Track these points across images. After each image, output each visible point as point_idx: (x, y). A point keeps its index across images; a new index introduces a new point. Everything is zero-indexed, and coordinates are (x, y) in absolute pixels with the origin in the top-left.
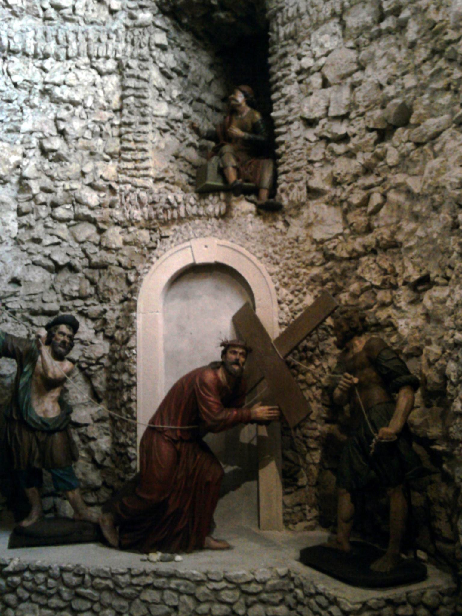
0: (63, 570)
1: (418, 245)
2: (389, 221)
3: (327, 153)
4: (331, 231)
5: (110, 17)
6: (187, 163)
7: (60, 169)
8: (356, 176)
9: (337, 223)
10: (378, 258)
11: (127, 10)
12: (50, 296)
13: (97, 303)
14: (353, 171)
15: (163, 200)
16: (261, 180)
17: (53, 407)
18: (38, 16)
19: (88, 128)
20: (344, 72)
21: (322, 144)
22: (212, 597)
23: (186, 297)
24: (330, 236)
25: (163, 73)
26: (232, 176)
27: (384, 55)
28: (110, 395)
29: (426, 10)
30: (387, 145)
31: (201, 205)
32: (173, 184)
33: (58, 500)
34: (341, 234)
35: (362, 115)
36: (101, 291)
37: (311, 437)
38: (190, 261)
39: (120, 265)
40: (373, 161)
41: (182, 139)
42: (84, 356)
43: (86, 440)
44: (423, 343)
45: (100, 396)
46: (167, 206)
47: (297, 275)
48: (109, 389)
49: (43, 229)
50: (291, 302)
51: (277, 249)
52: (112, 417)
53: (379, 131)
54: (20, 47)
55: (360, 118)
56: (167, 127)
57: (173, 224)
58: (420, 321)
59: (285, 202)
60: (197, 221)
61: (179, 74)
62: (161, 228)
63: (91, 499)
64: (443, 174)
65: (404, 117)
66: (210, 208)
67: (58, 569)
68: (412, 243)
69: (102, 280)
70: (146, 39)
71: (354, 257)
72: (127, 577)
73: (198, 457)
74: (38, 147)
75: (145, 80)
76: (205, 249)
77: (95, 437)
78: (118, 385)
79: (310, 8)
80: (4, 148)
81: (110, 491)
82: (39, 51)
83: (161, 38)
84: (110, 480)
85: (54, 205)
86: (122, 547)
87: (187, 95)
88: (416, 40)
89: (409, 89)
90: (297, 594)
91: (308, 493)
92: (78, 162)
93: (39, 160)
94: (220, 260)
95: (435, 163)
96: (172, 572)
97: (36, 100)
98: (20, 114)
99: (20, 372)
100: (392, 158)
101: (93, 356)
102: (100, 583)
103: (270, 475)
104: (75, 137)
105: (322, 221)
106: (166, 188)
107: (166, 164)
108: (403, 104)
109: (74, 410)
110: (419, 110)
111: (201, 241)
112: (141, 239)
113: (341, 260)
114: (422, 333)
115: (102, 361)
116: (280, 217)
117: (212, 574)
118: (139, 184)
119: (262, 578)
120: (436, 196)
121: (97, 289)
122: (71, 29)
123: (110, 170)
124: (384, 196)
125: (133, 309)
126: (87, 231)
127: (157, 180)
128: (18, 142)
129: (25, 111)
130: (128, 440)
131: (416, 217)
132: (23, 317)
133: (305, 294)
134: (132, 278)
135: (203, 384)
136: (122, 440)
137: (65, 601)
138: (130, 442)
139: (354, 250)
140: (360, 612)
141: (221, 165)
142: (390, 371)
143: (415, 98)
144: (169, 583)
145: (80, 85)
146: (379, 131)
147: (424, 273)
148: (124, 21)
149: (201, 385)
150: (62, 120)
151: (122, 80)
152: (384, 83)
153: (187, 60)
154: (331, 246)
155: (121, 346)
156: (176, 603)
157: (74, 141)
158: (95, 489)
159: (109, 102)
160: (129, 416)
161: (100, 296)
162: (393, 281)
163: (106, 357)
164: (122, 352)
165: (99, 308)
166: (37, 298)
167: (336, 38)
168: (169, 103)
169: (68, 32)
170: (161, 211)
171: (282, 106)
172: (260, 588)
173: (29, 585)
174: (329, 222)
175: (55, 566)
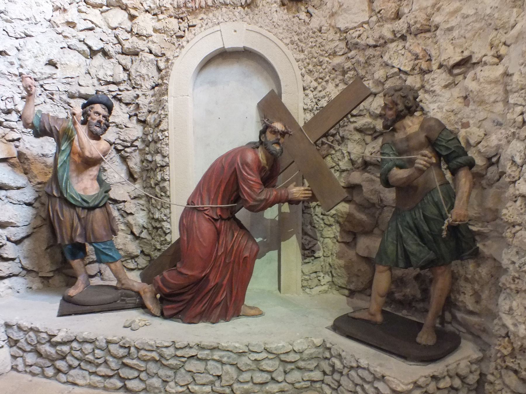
0: (108, 342)
4: (356, 20)
9: (363, 11)
10: (407, 45)
12: (85, 80)
13: (130, 88)
17: (92, 185)
22: (254, 366)
23: (213, 83)
24: (356, 25)
28: (144, 176)
34: (367, 23)
36: (134, 77)
38: (218, 46)
39: (151, 52)
43: (125, 215)
44: (459, 126)
45: (136, 176)
47: (321, 63)
48: (144, 170)
50: (315, 88)
51: (302, 37)
52: (147, 196)
57: (200, 13)
58: (457, 105)
60: (224, 9)
62: (188, 17)
63: (131, 265)
67: (105, 341)
69: (134, 66)
71: (381, 44)
73: (236, 235)
77: (133, 212)
78: (152, 166)
81: (148, 258)
86: (163, 316)
91: (322, 263)
94: (249, 45)
96: (215, 345)
101: (128, 139)
103: (291, 247)
109: (112, 189)
112: (170, 26)
114: (459, 116)
115: (135, 144)
119: (300, 348)
121: (129, 75)
125: (165, 92)
130: (162, 215)
132: (61, 99)
133: (327, 81)
134: (162, 65)
135: (245, 163)
136: (157, 216)
138: (165, 218)
142: (448, 150)
144: (212, 355)
147: (466, 54)
149: (242, 165)
154: (357, 34)
155: (154, 129)
158: (133, 257)
160: (163, 194)
161: (133, 82)
162: (424, 66)
163: (139, 140)
164: (155, 134)
165: (133, 93)
166: (74, 82)
172: (298, 357)
173: (78, 354)
175: (100, 338)
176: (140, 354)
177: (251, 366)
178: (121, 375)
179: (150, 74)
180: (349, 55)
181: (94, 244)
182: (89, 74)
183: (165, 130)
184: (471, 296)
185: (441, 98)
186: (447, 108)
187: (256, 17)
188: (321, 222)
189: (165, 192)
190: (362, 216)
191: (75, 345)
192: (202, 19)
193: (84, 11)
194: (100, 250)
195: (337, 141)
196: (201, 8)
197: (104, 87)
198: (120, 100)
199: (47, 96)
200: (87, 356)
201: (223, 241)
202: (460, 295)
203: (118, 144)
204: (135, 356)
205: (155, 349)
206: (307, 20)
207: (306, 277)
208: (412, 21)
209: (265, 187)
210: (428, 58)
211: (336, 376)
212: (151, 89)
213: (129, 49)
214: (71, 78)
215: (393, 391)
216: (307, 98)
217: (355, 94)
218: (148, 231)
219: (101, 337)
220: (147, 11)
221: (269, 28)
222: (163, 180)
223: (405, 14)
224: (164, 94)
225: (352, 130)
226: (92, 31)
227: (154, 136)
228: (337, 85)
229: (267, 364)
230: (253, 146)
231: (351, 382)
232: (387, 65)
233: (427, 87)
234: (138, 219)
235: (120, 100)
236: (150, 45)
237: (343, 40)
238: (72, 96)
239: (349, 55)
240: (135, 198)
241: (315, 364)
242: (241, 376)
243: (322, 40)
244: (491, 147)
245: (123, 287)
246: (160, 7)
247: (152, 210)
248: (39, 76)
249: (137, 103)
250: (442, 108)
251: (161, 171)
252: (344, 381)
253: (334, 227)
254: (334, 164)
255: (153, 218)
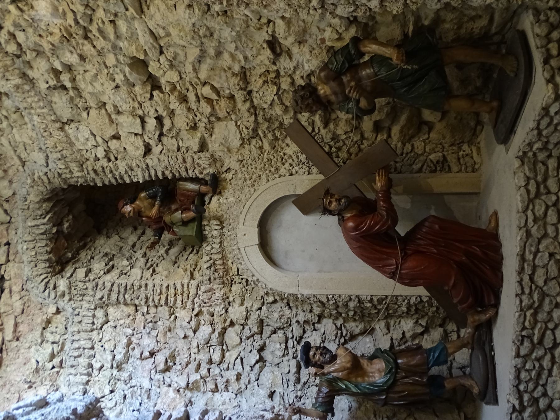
0: (518, 355)
1: (243, 52)
2: (224, 78)
3: (171, 135)
5: (62, 314)
6: (181, 254)
7: (182, 356)
8: (189, 109)
10: (255, 89)
11: (57, 299)
13: (291, 328)
14: (185, 111)
15: (208, 272)
16: (193, 191)
18: (58, 372)
19: (150, 333)
20: (107, 120)
21: (164, 139)
22: (541, 223)
24: (238, 131)
25: (109, 271)
26: (191, 214)
27: (92, 85)
28: (368, 319)
29: (53, 45)
30: (163, 81)
31: (212, 241)
32: (196, 266)
33: (455, 364)
34: (236, 123)
35: (140, 104)
37: (403, 149)
38: (257, 249)
39: (260, 309)
40: (176, 94)
41: (162, 258)
42: (334, 340)
43: (404, 340)
46: (212, 269)
47: (269, 160)
48: (362, 319)
49: (229, 371)
50: (291, 165)
51: (248, 177)
53: (153, 89)
54: (81, 387)
55: (143, 106)
56: (151, 269)
58: (306, 49)
59: (211, 170)
60: (225, 244)
61: (111, 260)
62: (231, 275)
63: (454, 336)
64: (183, 26)
65: (139, 64)
66: (215, 233)
67: (517, 359)
68: (241, 57)
69: (272, 324)
70: (81, 285)
71: (254, 110)
72: (524, 297)
74: (163, 374)
75: (112, 285)
76: (246, 235)
79: (57, 150)
80: (162, 402)
82: (85, 372)
83: (81, 273)
84: (439, 322)
85: (210, 362)
86: (497, 305)
87: (127, 254)
88: (78, 54)
89: (117, 60)
90: (537, 149)
91: (450, 152)
92: (175, 342)
93: (174, 374)
95: (174, 32)
96: (519, 258)
97: (125, 375)
98: (136, 388)
99: (347, 392)
100: (173, 76)
101: (335, 332)
102: (529, 321)
104: (156, 343)
105: (226, 139)
106: (199, 271)
107: (180, 270)
108: (130, 66)
110: (133, 51)
111: (240, 239)
113: (256, 121)
114: (315, 46)
115: (339, 326)
116: (223, 176)
117: (520, 223)
118: (195, 292)
119: (523, 180)
120: (201, 33)
121: (279, 329)
122: (70, 345)
123: (183, 315)
124: (204, 84)
125: (295, 296)
126: (232, 336)
127: (192, 277)
128: (158, 390)
129: (133, 385)
130: (404, 304)
131: (219, 54)
132: (301, 390)
133: (284, 154)
134: (271, 299)
135: (356, 229)
136: (404, 309)
137: (546, 354)
138: (406, 301)
139: (249, 111)
140: (556, 86)
141: (181, 223)
142: (344, 62)
143: (124, 55)
145: (114, 339)
146: (153, 89)
147: (265, 46)
148: (66, 302)
150: (141, 354)
151: (113, 305)
152: (114, 84)
153: (102, 254)
155: (326, 308)
156: (547, 255)
157: (159, 344)
158: (446, 335)
159: (129, 316)
160: (384, 302)
161: (286, 325)
162: (273, 75)
163: (335, 322)
164: (331, 307)
165: (295, 326)
167: (81, 127)
168: (132, 267)
169: (72, 348)
170: (216, 274)
171: (134, 174)
172: (532, 182)
173: (531, 386)
174: (226, 133)
176: (528, 327)
177: (540, 225)
178: (550, 346)
179: (279, 310)
180: (262, 135)
181: (430, 366)
182: (279, 364)
183: (328, 298)
184: (474, 22)
185: (300, 61)
186: (308, 57)
187: (232, 217)
188: (409, 155)
189: (383, 300)
190: (403, 119)
191: (522, 387)
192: (232, 263)
193: (227, 365)
194: (434, 362)
195: (335, 144)
196: (223, 263)
197: (290, 351)
198: (301, 338)
199: (298, 402)
200: (533, 377)
201: (424, 248)
202: (474, 32)
203: (339, 342)
204: (531, 331)
205: (523, 313)
206: (233, 172)
207: (463, 168)
208: (237, 87)
209: (376, 211)
210: (266, 73)
211: (551, 146)
212: (292, 310)
213: (258, 327)
214: (283, 379)
215: (556, 100)
216: (299, 172)
217: (297, 132)
218: (419, 319)
219: (513, 362)
220: (226, 311)
221: (242, 206)
222: (371, 301)
223: (230, 92)
224: (297, 298)
225: (326, 130)
226: (244, 359)
227: (332, 307)
228: (287, 145)
229: (538, 210)
230: (341, 221)
231: (554, 134)
232: (271, 104)
233: (290, 72)
234: (408, 328)
235: (301, 338)
236: (254, 309)
237: (249, 142)
238: (298, 380)
239: (262, 135)
240: (388, 329)
241: (541, 164)
242: (551, 234)
243: (250, 159)
244: (341, 23)
245: (471, 342)
246: (223, 299)
247: (399, 314)
248: (282, 407)
249: (304, 322)
250: (308, 60)
251: (363, 303)
252: (554, 139)
253: (414, 143)
254: (356, 145)
255: (407, 313)
